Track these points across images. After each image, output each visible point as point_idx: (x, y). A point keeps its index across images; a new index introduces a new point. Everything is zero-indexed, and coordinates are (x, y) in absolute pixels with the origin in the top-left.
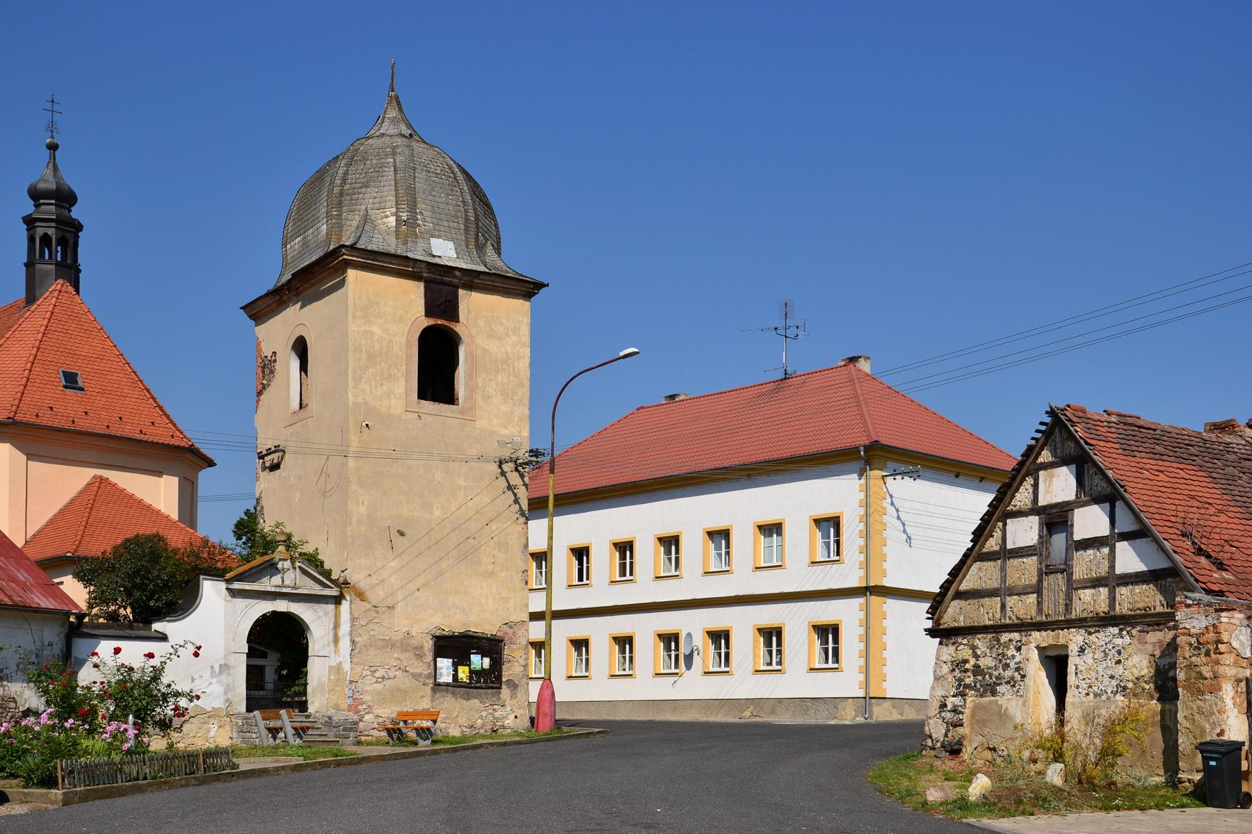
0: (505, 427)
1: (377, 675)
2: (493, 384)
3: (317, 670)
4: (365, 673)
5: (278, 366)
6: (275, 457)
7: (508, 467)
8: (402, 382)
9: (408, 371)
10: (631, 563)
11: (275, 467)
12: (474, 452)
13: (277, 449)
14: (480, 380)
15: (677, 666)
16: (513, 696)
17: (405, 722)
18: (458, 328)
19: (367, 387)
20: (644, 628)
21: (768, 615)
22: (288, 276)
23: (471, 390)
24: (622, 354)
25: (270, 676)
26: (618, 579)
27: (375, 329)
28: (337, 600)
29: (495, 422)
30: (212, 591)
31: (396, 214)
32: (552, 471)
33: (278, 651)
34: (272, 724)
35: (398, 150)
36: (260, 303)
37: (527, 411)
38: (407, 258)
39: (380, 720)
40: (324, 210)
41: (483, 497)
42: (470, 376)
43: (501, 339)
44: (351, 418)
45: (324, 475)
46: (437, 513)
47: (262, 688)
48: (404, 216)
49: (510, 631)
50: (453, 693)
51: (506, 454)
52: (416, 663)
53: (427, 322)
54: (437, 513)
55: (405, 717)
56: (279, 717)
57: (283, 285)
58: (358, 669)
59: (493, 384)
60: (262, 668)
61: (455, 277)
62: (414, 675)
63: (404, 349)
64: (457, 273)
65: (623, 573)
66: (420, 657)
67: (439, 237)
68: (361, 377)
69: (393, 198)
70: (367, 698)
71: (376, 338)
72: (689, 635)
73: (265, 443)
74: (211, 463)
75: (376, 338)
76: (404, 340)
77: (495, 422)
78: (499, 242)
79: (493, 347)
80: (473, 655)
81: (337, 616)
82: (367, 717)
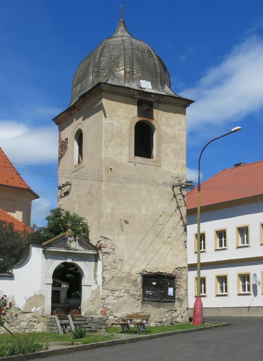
0: (175, 170)
1: (115, 295)
2: (170, 149)
3: (86, 293)
4: (109, 294)
5: (69, 145)
6: (68, 187)
7: (177, 190)
8: (127, 148)
9: (130, 143)
10: (204, 244)
11: (67, 193)
12: (161, 181)
13: (68, 184)
14: (163, 147)
15: (249, 290)
16: (181, 306)
17: (131, 320)
18: (154, 122)
19: (111, 150)
20: (232, 273)
21: (221, 272)
22: (76, 99)
23: (159, 151)
24: (233, 130)
25: (63, 295)
26: (219, 248)
27: (115, 122)
28: (96, 258)
29: (170, 167)
30: (36, 252)
31: (124, 69)
32: (199, 190)
33: (68, 281)
34: (64, 321)
35: (125, 41)
36: (61, 116)
37: (185, 162)
38: (130, 88)
39: (117, 319)
40: (91, 70)
41: (162, 206)
42: (159, 145)
43: (172, 127)
44: (103, 165)
45: (90, 194)
46: (144, 212)
47: (59, 302)
48: (128, 70)
49: (179, 272)
50: (152, 305)
51: (176, 182)
52: (133, 288)
53: (138, 119)
54: (144, 212)
55: (131, 318)
56: (67, 319)
57: (72, 107)
58: (106, 292)
59: (170, 149)
60: (58, 292)
61: (151, 98)
62: (132, 295)
63: (128, 132)
64: (153, 96)
65: (221, 245)
66: (136, 285)
67: (144, 79)
68: (108, 146)
69: (123, 62)
70: (110, 307)
71: (115, 126)
72: (255, 275)
73: (62, 181)
74: (37, 197)
75: (115, 126)
76: (128, 128)
77: (170, 167)
78: (170, 84)
79: (169, 131)
80: (158, 286)
81: (96, 266)
82: (110, 317)
